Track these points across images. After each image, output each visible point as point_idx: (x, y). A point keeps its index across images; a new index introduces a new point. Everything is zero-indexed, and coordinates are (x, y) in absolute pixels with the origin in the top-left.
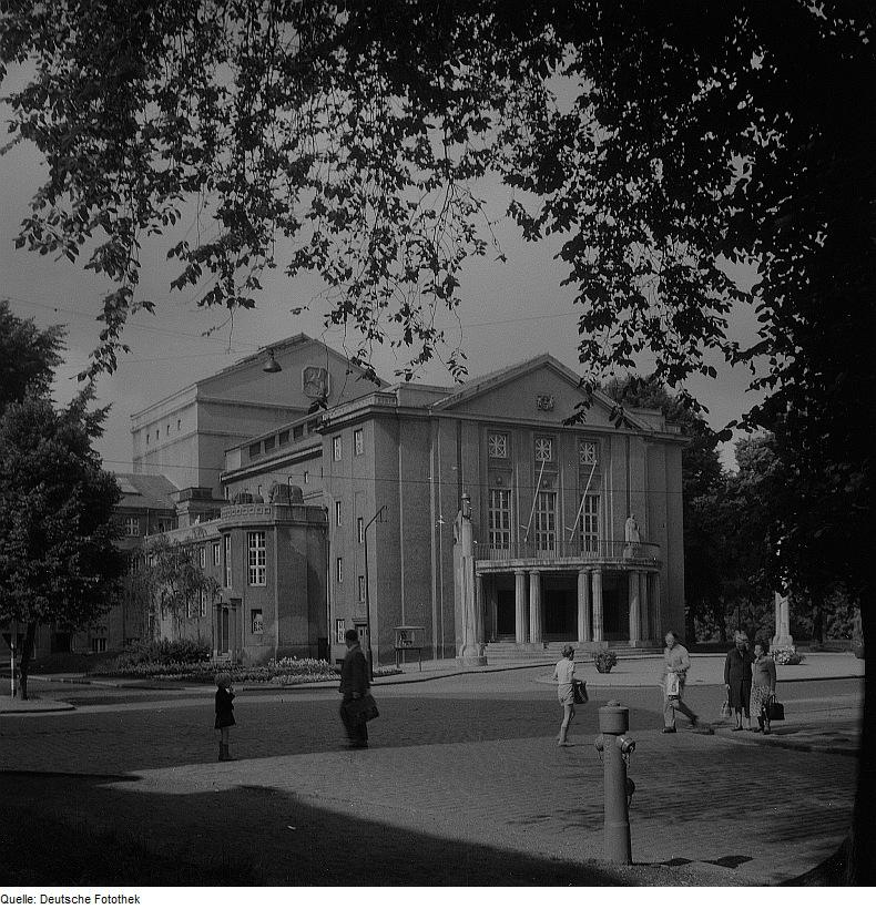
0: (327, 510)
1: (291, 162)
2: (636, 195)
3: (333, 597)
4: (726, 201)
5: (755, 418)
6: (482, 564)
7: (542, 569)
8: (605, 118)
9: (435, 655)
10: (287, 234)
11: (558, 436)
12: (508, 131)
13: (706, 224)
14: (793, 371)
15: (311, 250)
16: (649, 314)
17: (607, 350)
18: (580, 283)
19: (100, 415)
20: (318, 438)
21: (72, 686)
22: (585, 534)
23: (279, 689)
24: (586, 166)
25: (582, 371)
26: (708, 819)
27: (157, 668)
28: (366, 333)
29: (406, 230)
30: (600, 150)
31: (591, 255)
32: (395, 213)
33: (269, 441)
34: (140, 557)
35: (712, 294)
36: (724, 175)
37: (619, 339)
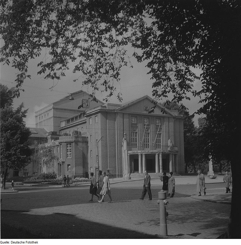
0: (88, 138)
1: (73, 41)
2: (168, 50)
3: (89, 161)
4: (193, 51)
5: (201, 111)
6: (130, 152)
7: (146, 153)
8: (160, 28)
9: (117, 177)
10: (72, 61)
11: (150, 118)
12: (134, 33)
13: (188, 58)
14: (212, 97)
15: (79, 66)
16: (172, 83)
17: (160, 93)
18: (152, 74)
19: (25, 112)
20: (85, 118)
21: (18, 185)
22: (157, 144)
23: (74, 186)
24: (155, 41)
25: (153, 98)
26: (189, 222)
27: (41, 180)
28: (94, 88)
29: (106, 59)
30: (159, 37)
31: (156, 66)
32: (103, 54)
33: (72, 119)
34: (37, 151)
35: (189, 77)
36: (192, 44)
37: (164, 89)
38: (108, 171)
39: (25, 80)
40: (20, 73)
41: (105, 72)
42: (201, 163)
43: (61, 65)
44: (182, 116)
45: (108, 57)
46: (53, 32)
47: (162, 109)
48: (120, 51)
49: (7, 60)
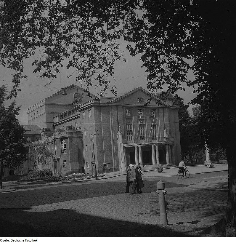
0: (82, 132)
3: (85, 156)
4: (185, 42)
5: (194, 101)
6: (125, 145)
8: (151, 21)
12: (125, 25)
14: (204, 87)
15: (73, 61)
16: (165, 74)
17: (155, 85)
19: (18, 109)
20: (79, 113)
22: (153, 135)
25: (148, 90)
27: (38, 178)
29: (98, 54)
31: (149, 59)
32: (96, 49)
33: (65, 114)
35: (182, 68)
37: (158, 81)
38: (105, 165)
39: (21, 81)
40: (16, 73)
41: (98, 66)
42: (198, 152)
43: (55, 62)
44: (176, 106)
45: (101, 51)
46: (45, 29)
47: (157, 100)
48: (112, 45)
49: (3, 62)
